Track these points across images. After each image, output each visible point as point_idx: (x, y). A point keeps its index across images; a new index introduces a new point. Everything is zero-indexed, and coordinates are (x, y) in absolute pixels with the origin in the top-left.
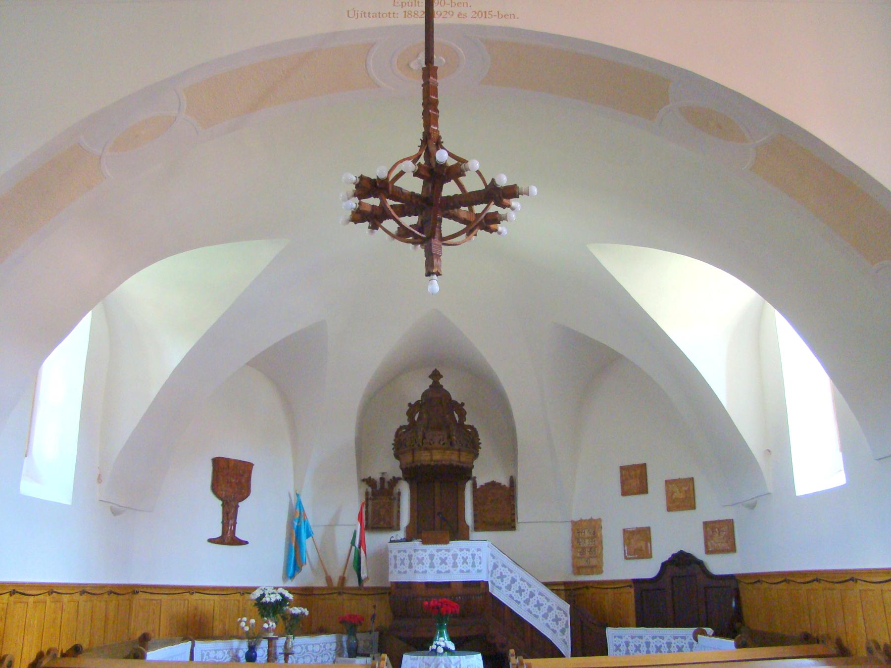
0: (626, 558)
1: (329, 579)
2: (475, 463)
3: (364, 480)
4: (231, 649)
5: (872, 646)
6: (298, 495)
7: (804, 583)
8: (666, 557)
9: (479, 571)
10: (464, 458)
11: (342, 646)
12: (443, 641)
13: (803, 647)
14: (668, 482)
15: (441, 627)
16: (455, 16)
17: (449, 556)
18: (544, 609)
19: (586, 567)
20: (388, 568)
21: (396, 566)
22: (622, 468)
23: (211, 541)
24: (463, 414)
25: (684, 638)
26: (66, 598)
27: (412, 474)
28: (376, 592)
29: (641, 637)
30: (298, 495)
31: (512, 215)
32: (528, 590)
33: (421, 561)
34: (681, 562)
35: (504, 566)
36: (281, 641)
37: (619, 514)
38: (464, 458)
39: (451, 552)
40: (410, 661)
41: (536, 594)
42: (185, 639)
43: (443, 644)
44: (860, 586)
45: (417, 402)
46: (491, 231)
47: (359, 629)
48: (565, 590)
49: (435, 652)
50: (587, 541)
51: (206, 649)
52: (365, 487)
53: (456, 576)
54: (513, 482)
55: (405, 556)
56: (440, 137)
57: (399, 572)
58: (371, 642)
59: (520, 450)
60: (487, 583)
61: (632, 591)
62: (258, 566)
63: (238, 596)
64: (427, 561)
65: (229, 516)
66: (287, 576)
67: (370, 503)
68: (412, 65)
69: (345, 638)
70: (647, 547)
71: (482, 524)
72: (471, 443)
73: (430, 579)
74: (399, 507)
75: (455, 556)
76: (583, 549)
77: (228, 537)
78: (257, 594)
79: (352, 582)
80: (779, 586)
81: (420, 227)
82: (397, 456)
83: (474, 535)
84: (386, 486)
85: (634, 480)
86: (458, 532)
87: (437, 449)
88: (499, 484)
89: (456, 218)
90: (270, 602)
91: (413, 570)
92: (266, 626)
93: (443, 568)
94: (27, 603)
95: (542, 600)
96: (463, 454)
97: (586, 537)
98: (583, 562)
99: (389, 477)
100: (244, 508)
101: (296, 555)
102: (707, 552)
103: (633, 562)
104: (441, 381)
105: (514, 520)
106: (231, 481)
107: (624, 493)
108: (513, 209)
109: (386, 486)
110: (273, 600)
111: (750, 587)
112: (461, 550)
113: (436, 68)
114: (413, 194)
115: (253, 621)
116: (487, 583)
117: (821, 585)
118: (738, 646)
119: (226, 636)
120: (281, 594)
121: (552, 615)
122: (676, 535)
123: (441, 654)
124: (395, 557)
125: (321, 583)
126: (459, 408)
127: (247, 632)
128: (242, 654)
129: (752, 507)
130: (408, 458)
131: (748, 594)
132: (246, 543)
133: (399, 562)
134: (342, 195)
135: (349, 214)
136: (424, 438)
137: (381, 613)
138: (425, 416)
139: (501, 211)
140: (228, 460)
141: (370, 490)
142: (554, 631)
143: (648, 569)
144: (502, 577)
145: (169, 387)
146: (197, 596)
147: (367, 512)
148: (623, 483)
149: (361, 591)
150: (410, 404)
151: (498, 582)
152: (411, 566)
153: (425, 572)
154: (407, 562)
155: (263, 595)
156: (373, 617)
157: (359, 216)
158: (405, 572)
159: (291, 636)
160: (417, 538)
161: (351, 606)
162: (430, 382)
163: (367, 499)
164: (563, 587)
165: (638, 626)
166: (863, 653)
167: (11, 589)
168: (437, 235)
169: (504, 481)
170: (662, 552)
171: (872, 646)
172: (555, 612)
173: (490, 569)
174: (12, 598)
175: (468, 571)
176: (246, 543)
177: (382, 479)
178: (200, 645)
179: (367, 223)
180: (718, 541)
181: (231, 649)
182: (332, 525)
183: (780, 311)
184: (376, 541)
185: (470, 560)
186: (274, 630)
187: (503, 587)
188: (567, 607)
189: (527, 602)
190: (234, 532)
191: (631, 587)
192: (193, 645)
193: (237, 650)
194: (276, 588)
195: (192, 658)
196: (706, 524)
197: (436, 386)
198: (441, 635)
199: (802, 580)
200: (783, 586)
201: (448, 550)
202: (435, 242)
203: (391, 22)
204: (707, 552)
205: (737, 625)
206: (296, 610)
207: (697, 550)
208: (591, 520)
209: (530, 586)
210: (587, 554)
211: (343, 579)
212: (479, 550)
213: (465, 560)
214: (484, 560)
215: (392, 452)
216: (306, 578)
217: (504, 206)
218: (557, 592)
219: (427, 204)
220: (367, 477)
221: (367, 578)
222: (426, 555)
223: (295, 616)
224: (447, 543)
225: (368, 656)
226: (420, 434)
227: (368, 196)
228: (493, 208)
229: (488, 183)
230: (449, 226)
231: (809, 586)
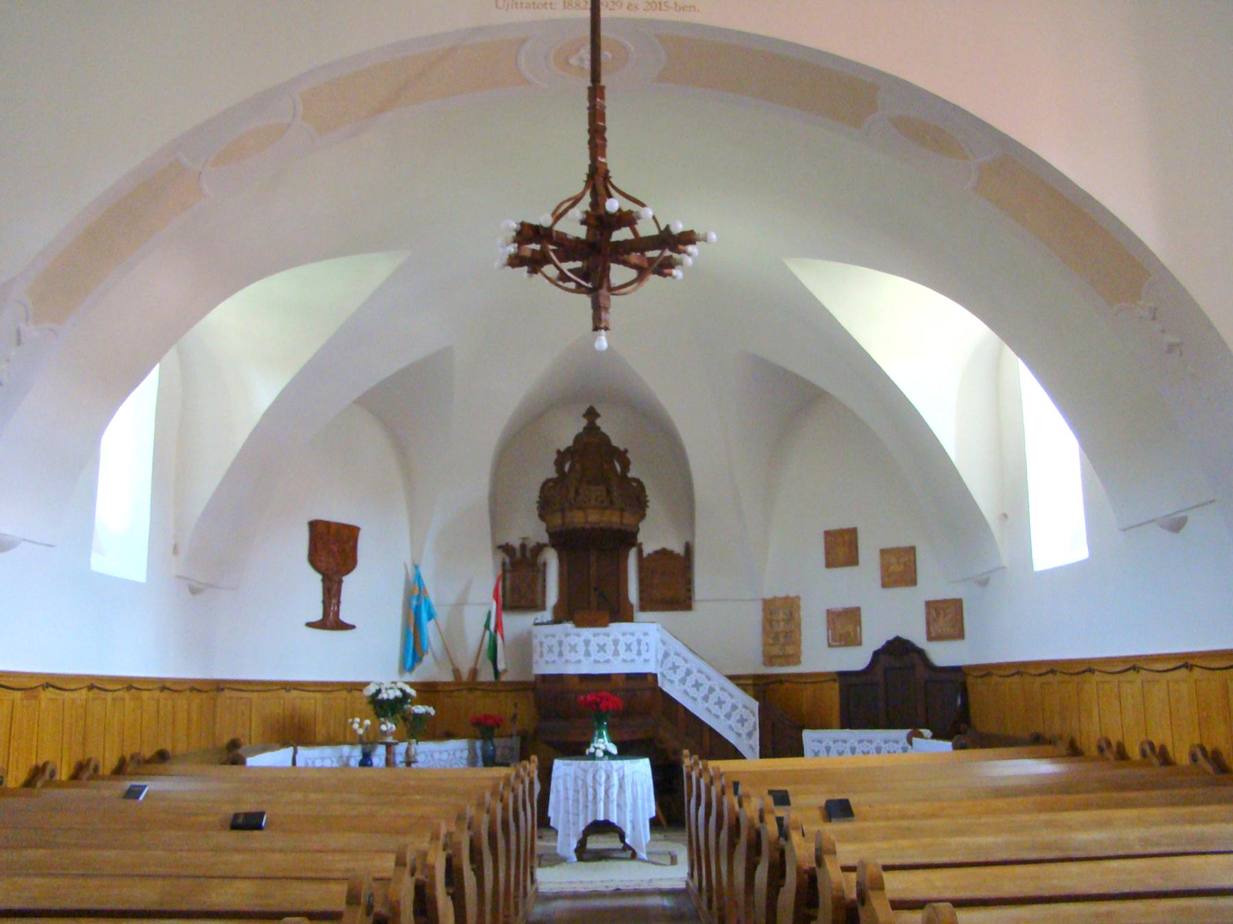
0: (830, 646)
1: (456, 672)
2: (642, 526)
3: (500, 547)
4: (341, 757)
5: (1104, 745)
6: (416, 567)
7: (1040, 675)
8: (878, 644)
9: (646, 661)
10: (628, 519)
11: (476, 754)
12: (603, 743)
13: (1035, 748)
14: (884, 552)
15: (600, 726)
16: (625, 7)
17: (609, 641)
18: (726, 708)
19: (780, 657)
20: (531, 656)
21: (542, 655)
22: (827, 533)
23: (310, 625)
24: (626, 465)
25: (897, 742)
26: (145, 695)
27: (563, 540)
28: (520, 687)
29: (845, 741)
30: (416, 567)
31: (688, 261)
32: (707, 684)
33: (573, 648)
34: (898, 651)
35: (677, 654)
36: (401, 748)
37: (822, 591)
38: (628, 519)
39: (612, 638)
40: (563, 768)
41: (717, 689)
42: (285, 744)
43: (602, 747)
44: (1097, 677)
45: (568, 449)
46: (665, 275)
47: (496, 731)
48: (754, 685)
49: (593, 757)
50: (782, 624)
51: (311, 757)
52: (502, 556)
53: (618, 666)
54: (689, 549)
55: (553, 642)
56: (607, 172)
57: (547, 662)
58: (511, 749)
59: (698, 513)
60: (655, 676)
61: (836, 686)
62: (368, 655)
63: (344, 694)
64: (581, 648)
65: (332, 594)
66: (405, 668)
67: (508, 575)
68: (573, 61)
69: (478, 744)
70: (855, 631)
71: (651, 602)
72: (636, 500)
73: (585, 669)
74: (544, 580)
75: (616, 642)
76: (777, 634)
77: (331, 621)
78: (371, 689)
79: (486, 675)
80: (1010, 679)
81: (584, 274)
82: (542, 517)
83: (639, 615)
84: (528, 554)
85: (842, 548)
86: (621, 613)
87: (595, 508)
88: (672, 552)
89: (626, 263)
90: (388, 700)
91: (563, 659)
92: (384, 728)
93: (601, 656)
94: (105, 699)
95: (724, 696)
96: (627, 515)
97: (780, 619)
98: (776, 650)
99: (531, 544)
100: (351, 584)
101: (415, 642)
102: (930, 638)
103: (835, 649)
104: (599, 422)
105: (690, 598)
106: (333, 549)
107: (830, 564)
108: (689, 255)
109: (528, 554)
110: (392, 697)
111: (979, 680)
112: (624, 634)
113: (603, 88)
114: (578, 239)
115: (367, 722)
116: (655, 676)
117: (1059, 677)
118: (955, 747)
119: (330, 741)
120: (401, 690)
121: (736, 716)
122: (893, 617)
123: (601, 759)
124: (541, 644)
125: (449, 678)
126: (622, 456)
127: (361, 736)
128: (354, 763)
129: (984, 583)
130: (557, 520)
131: (976, 687)
132: (353, 627)
133: (545, 650)
134: (500, 241)
135: (505, 259)
136: (577, 493)
137: (524, 714)
138: (578, 467)
139: (675, 256)
140: (328, 524)
141: (507, 560)
142: (739, 735)
143: (856, 659)
144: (674, 668)
145: (261, 433)
146: (294, 693)
147: (504, 587)
148: (828, 553)
149: (498, 686)
150: (559, 452)
151: (670, 675)
152: (561, 654)
153: (579, 662)
154: (556, 649)
155: (379, 691)
156: (514, 717)
157: (516, 261)
158: (554, 662)
159: (414, 741)
160: (568, 620)
161: (484, 706)
162: (584, 422)
163: (504, 571)
164: (750, 682)
165: (843, 727)
166: (1094, 751)
167: (88, 683)
168: (605, 285)
169: (678, 549)
170: (874, 637)
171: (1104, 745)
172: (741, 710)
173: (660, 657)
174: (91, 694)
175: (633, 661)
176: (353, 627)
177: (523, 546)
178: (301, 750)
179: (526, 268)
180: (943, 625)
181: (341, 757)
182: (460, 604)
183: (1010, 346)
184: (517, 623)
185: (634, 647)
186: (392, 733)
187: (676, 681)
188: (755, 705)
189: (706, 698)
190: (337, 613)
191: (834, 680)
192: (295, 752)
193: (349, 758)
194: (395, 683)
195: (294, 763)
196: (928, 604)
197: (591, 428)
198: (601, 736)
199: (1038, 672)
200: (1016, 679)
201: (607, 635)
202: (603, 291)
203: (546, 14)
204: (930, 638)
205: (963, 726)
206: (420, 709)
207: (917, 636)
208: (786, 598)
209: (709, 678)
210: (782, 639)
211: (474, 672)
212: (645, 634)
213: (628, 648)
214: (652, 649)
215: (537, 513)
216: (429, 670)
217: (679, 252)
218: (744, 688)
219: (596, 249)
220: (503, 543)
221: (505, 671)
222: (579, 641)
223: (418, 716)
224: (605, 625)
225: (507, 765)
226: (572, 490)
227: (529, 241)
228: (668, 253)
229: (663, 227)
230: (619, 274)
231: (1043, 679)
